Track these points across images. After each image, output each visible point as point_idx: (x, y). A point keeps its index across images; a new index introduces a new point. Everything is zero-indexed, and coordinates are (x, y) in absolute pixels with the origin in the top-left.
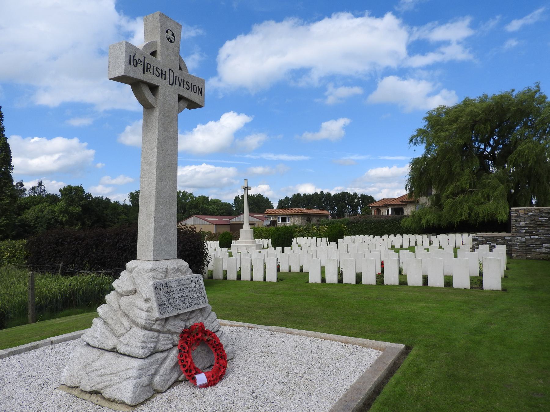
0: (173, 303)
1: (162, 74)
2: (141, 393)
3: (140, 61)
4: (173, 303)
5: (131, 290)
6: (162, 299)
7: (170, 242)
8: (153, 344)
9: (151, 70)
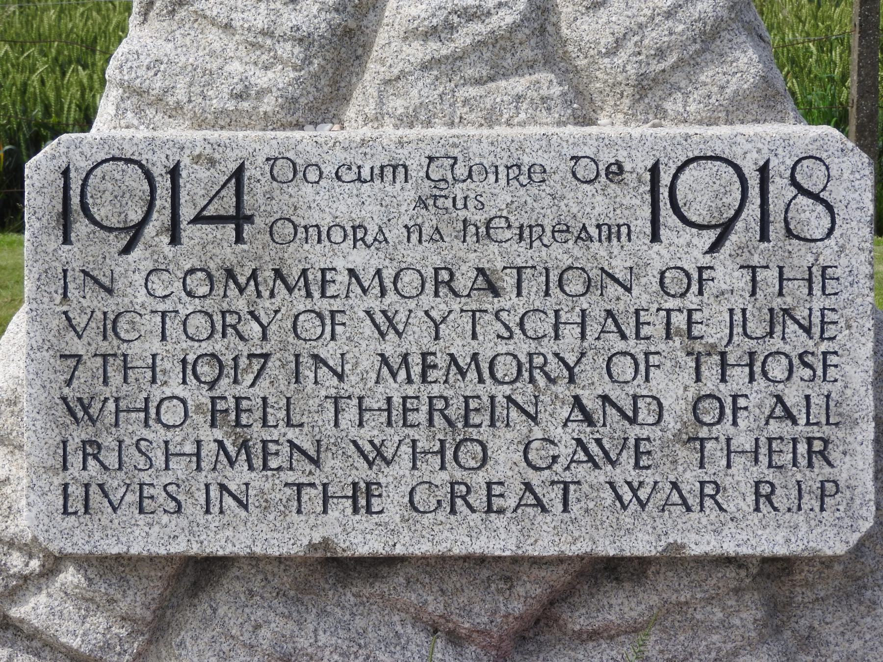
0: (276, 415)
4: (276, 415)
6: (134, 349)
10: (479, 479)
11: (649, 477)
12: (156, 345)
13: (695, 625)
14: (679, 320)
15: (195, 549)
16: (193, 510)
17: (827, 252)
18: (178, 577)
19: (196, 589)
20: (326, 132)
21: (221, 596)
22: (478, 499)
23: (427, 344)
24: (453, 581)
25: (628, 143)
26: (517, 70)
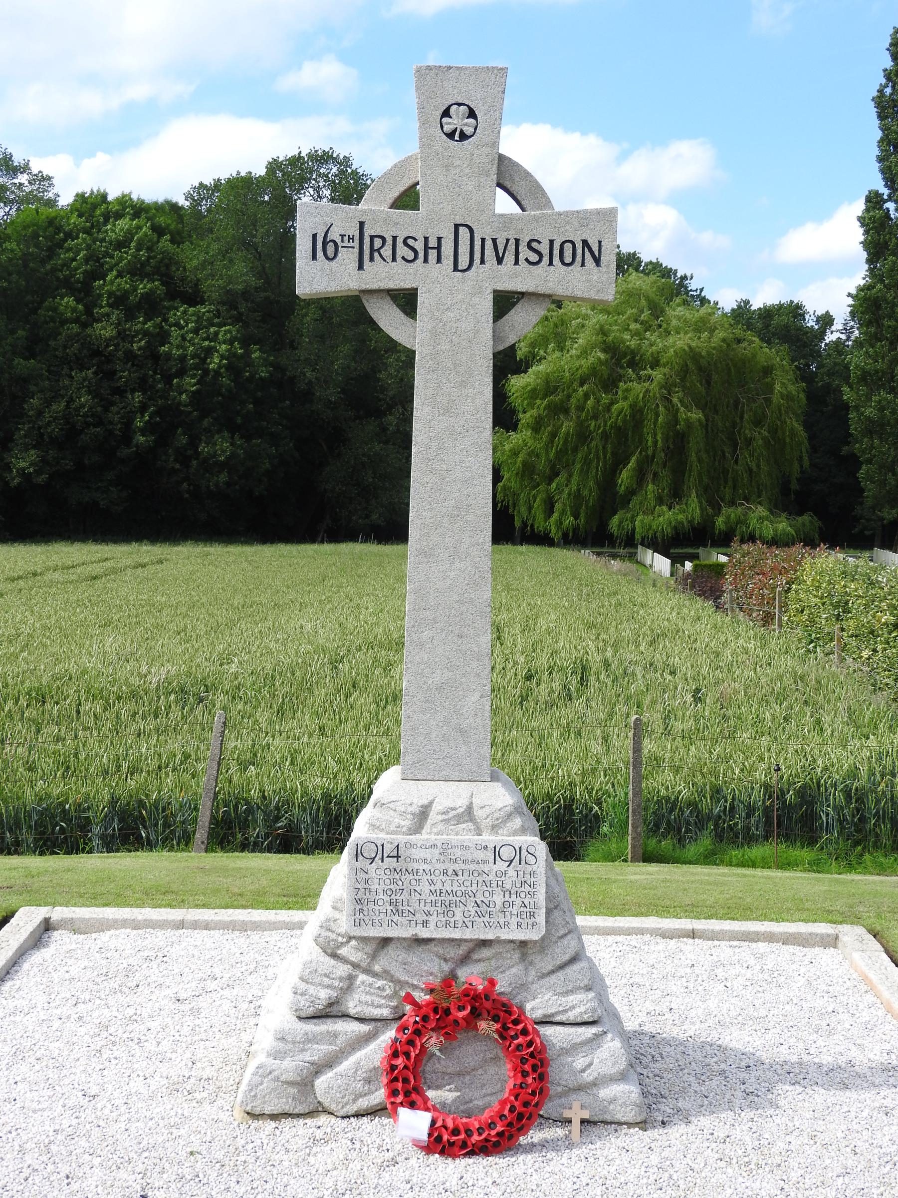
0: (405, 903)
1: (426, 248)
2: (270, 1092)
3: (346, 238)
4: (405, 903)
5: (673, 804)
6: (372, 887)
7: (462, 732)
8: (328, 991)
9: (387, 252)
10: (452, 920)
11: (492, 920)
12: (377, 886)
13: (504, 958)
14: (500, 883)
15: (385, 935)
16: (385, 926)
17: (535, 868)
18: (379, 944)
19: (383, 947)
20: (418, 836)
21: (390, 948)
22: (452, 925)
23: (441, 887)
24: (446, 945)
25: (489, 841)
26: (463, 823)
